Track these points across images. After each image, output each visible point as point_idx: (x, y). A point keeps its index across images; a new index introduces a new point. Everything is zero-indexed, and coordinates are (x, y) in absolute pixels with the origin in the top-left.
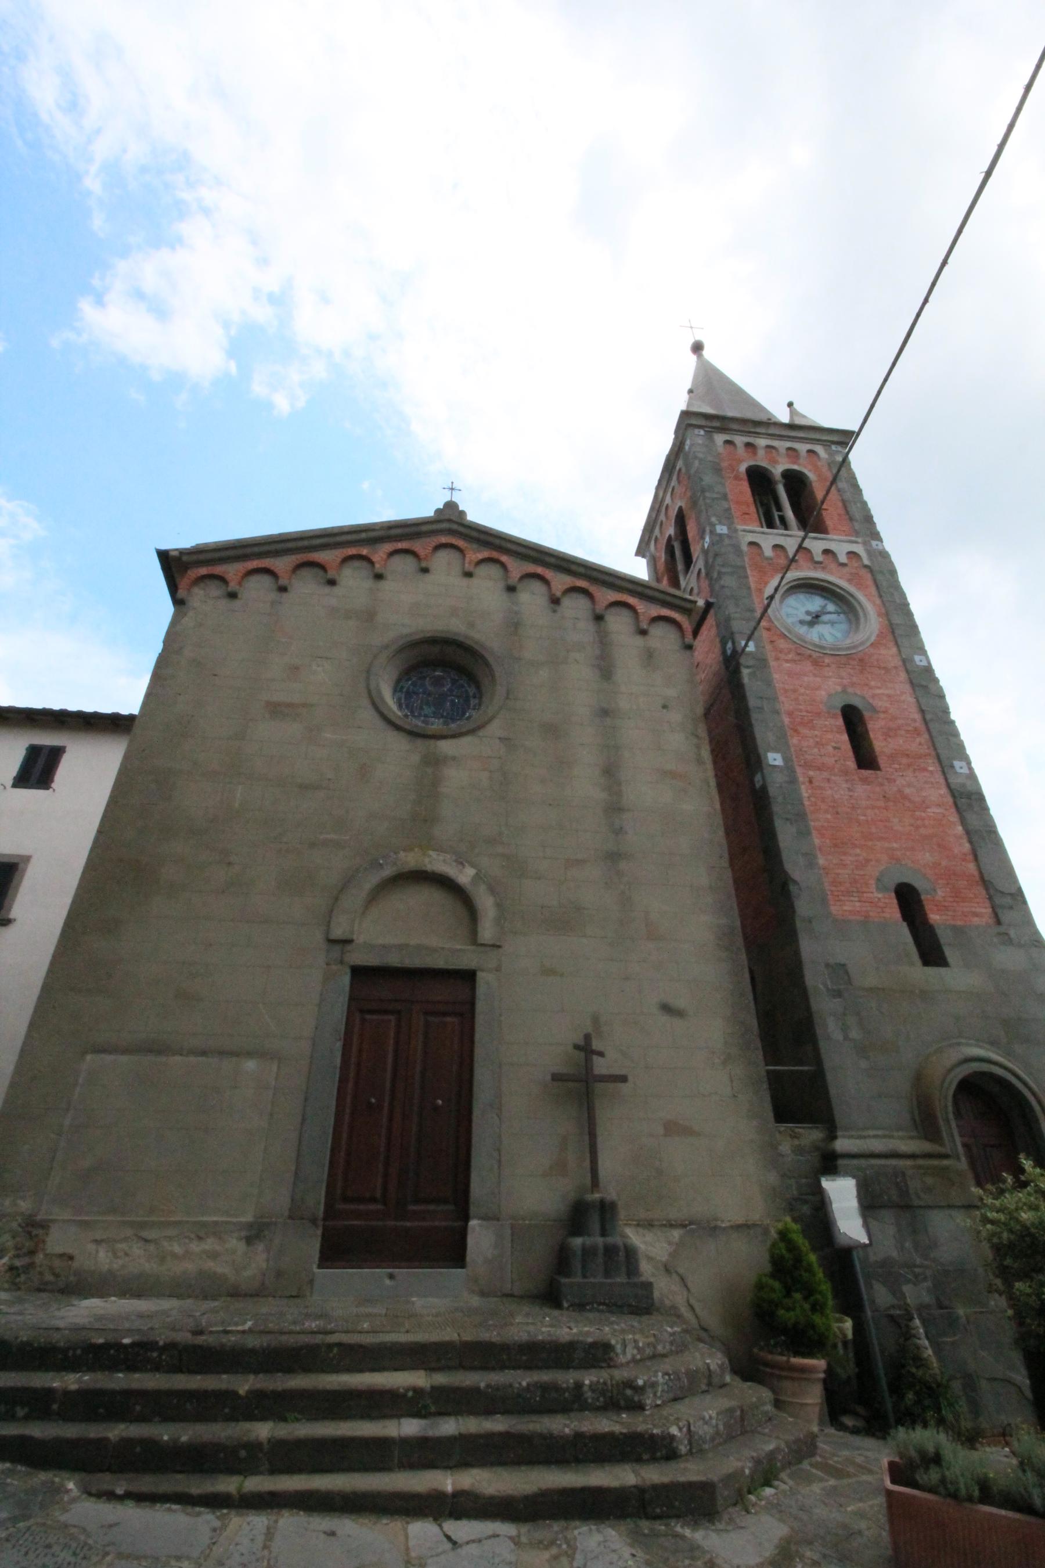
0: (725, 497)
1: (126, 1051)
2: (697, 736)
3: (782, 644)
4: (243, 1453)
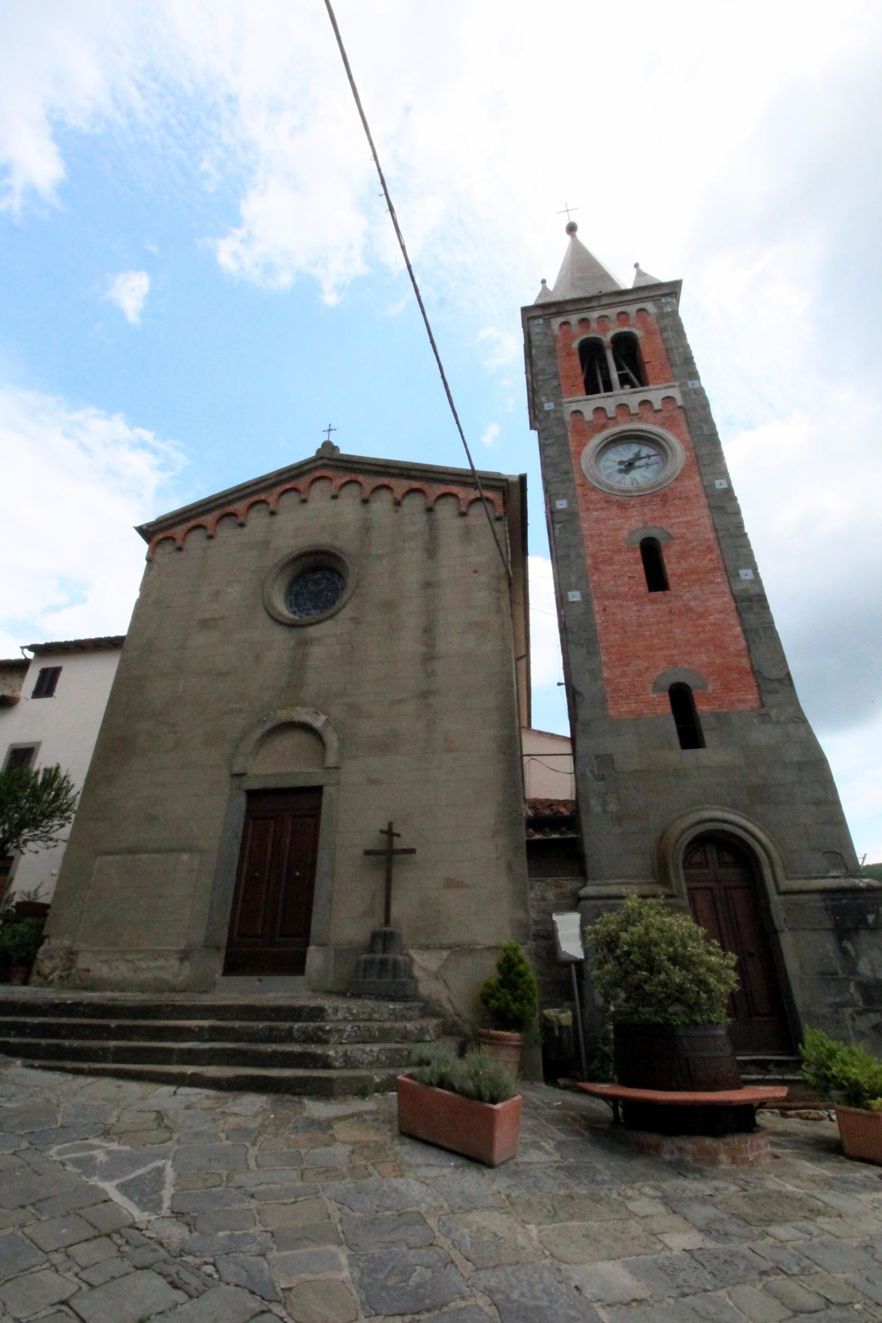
0: (556, 376)
1: (120, 853)
2: (499, 591)
3: (593, 496)
4: (101, 1053)
